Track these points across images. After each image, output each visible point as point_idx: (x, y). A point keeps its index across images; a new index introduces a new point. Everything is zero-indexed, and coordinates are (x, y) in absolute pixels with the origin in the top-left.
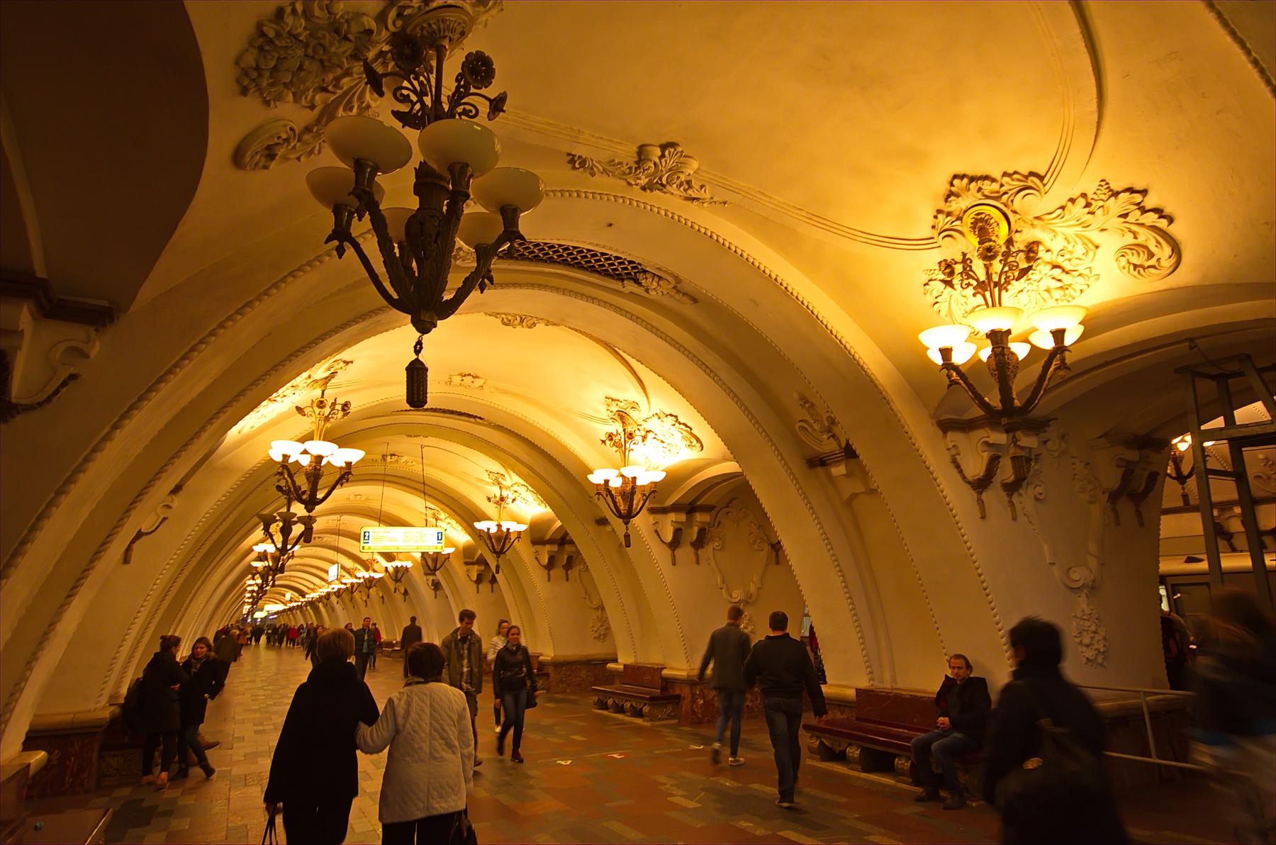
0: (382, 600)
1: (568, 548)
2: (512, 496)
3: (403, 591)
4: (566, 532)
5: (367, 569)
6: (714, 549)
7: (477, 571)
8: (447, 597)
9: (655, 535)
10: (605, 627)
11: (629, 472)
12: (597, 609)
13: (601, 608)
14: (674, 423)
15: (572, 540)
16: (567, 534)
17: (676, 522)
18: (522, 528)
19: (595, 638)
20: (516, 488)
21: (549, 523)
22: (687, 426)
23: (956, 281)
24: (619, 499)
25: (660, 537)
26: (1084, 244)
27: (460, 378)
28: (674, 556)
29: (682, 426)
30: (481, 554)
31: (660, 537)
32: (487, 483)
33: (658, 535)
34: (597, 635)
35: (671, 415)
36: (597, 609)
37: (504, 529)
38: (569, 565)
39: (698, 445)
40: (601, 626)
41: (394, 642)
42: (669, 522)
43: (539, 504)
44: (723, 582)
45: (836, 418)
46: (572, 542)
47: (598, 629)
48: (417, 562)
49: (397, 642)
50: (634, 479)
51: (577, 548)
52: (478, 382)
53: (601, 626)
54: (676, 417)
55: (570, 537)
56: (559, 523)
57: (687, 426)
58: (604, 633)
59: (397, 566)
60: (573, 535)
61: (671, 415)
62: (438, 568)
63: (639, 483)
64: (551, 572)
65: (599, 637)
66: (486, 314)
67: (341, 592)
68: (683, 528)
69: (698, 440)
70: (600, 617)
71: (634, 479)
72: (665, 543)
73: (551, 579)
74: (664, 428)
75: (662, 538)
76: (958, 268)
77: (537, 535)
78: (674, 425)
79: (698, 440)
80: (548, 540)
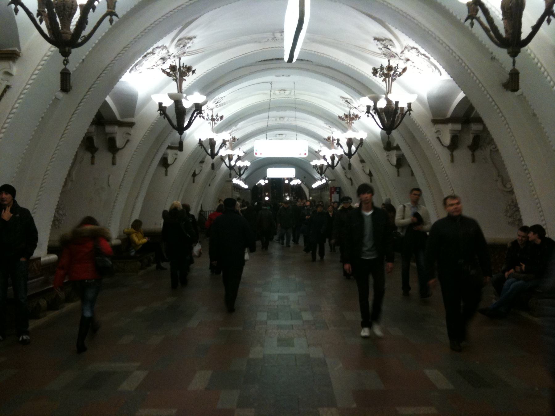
0: (369, 177)
1: (475, 127)
2: (402, 66)
3: (368, 172)
4: (471, 104)
5: (330, 147)
6: (491, 150)
8: (413, 174)
9: (363, 171)
14: (418, 54)
16: (471, 108)
17: (454, 130)
18: (412, 99)
20: (407, 54)
22: (427, 57)
25: (441, 142)
26: (395, 76)
27: (279, 92)
28: (452, 156)
31: (441, 142)
32: (374, 53)
33: (440, 140)
34: (510, 220)
37: (337, 145)
42: (448, 130)
44: (499, 176)
45: (496, 56)
46: (479, 120)
48: (451, 80)
50: (397, 103)
51: (484, 126)
52: (287, 92)
54: (417, 49)
55: (476, 111)
56: (461, 95)
57: (427, 57)
60: (481, 110)
62: (335, 164)
63: (400, 105)
66: (276, 76)
67: (324, 168)
68: (459, 135)
69: (436, 67)
71: (397, 103)
72: (445, 146)
75: (443, 143)
79: (436, 67)
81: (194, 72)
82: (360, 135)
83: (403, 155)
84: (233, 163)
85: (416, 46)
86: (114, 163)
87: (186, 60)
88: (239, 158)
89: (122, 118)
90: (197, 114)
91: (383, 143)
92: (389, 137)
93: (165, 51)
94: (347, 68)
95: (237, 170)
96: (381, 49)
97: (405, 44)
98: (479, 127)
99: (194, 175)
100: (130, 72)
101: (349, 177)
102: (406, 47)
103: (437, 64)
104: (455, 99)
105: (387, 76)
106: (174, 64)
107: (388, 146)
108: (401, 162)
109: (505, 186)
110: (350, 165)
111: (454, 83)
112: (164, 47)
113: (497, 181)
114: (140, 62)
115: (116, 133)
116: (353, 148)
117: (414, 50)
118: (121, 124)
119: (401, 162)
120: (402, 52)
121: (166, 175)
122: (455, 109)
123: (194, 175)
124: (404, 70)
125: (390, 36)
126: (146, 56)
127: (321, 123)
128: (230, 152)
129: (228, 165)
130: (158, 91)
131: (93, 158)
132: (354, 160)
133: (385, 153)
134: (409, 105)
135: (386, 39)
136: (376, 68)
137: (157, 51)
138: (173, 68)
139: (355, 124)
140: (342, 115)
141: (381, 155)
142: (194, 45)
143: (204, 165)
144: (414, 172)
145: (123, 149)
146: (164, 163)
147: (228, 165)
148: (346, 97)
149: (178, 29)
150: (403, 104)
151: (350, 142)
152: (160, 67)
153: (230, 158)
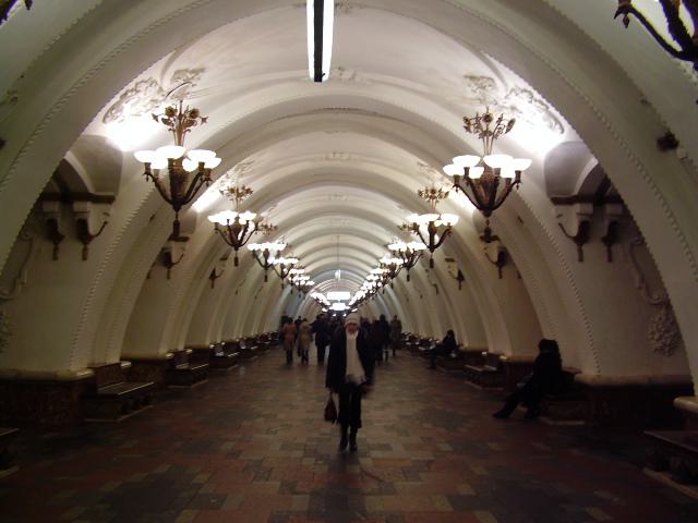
1: (610, 209)
3: (456, 275)
5: (423, 210)
7: (578, 214)
8: (520, 277)
10: (672, 333)
11: (493, 161)
12: (659, 305)
13: (666, 304)
15: (619, 196)
16: (606, 182)
17: (581, 214)
18: (523, 165)
19: (656, 350)
21: (580, 163)
23: (472, 128)
24: (481, 190)
25: (564, 232)
28: (580, 252)
29: (538, 104)
30: (597, 170)
31: (564, 232)
33: (562, 228)
34: (659, 345)
35: (526, 91)
36: (659, 305)
38: (611, 239)
39: (558, 126)
40: (667, 331)
41: (484, 353)
43: (551, 127)
44: (642, 280)
46: (617, 199)
47: (661, 336)
49: (489, 354)
51: (625, 208)
53: (667, 331)
54: (530, 93)
55: (614, 188)
56: (593, 162)
58: (673, 343)
59: (498, 171)
60: (622, 185)
61: (526, 91)
63: (504, 175)
64: (613, 248)
65: (662, 349)
70: (664, 318)
73: (503, 274)
74: (522, 102)
76: (473, 122)
77: (559, 189)
78: (530, 102)
79: (557, 121)
80: (575, 196)
81: (204, 120)
82: (449, 219)
83: (505, 248)
84: (270, 261)
85: (530, 88)
86: (169, 278)
87: (189, 104)
88: (278, 255)
89: (97, 190)
90: (202, 182)
91: (479, 232)
92: (488, 223)
93: (154, 89)
94: (437, 126)
95: (279, 270)
96: (475, 92)
97: (511, 85)
98: (616, 209)
99: (213, 276)
100: (104, 121)
101: (434, 282)
102: (512, 90)
103: (561, 119)
104: (582, 169)
105: (486, 134)
106: (174, 107)
107: (487, 236)
108: (503, 259)
109: (649, 295)
110: (432, 261)
111: (584, 146)
112: (153, 83)
113: (640, 288)
114: (118, 103)
115: (89, 212)
116: (437, 239)
117: (525, 94)
118: (97, 200)
119: (503, 259)
120: (506, 97)
121: (85, 258)
122: (588, 176)
123: (213, 276)
124: (511, 123)
125: (493, 75)
126: (126, 94)
127: (394, 205)
128: (263, 247)
129: (263, 263)
130: (153, 147)
131: (56, 250)
132: (438, 255)
133: (482, 245)
134: (518, 173)
135: (483, 77)
136: (469, 118)
137: (143, 86)
138: (170, 112)
139: (440, 205)
140: (423, 189)
141: (475, 247)
142: (202, 83)
143: (227, 263)
144: (522, 274)
145: (100, 237)
146: (166, 259)
147: (263, 263)
148: (478, 74)
149: (170, 55)
150: (508, 173)
151: (432, 229)
152: (150, 112)
153: (267, 254)
